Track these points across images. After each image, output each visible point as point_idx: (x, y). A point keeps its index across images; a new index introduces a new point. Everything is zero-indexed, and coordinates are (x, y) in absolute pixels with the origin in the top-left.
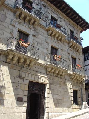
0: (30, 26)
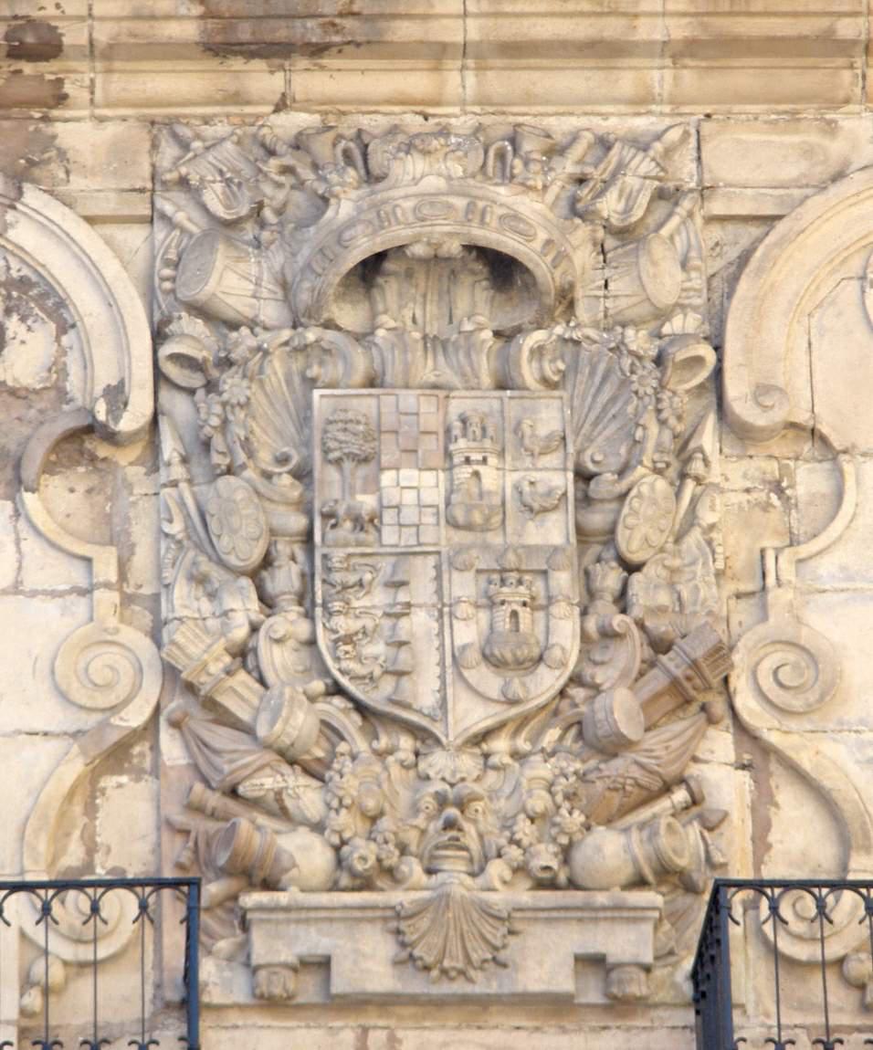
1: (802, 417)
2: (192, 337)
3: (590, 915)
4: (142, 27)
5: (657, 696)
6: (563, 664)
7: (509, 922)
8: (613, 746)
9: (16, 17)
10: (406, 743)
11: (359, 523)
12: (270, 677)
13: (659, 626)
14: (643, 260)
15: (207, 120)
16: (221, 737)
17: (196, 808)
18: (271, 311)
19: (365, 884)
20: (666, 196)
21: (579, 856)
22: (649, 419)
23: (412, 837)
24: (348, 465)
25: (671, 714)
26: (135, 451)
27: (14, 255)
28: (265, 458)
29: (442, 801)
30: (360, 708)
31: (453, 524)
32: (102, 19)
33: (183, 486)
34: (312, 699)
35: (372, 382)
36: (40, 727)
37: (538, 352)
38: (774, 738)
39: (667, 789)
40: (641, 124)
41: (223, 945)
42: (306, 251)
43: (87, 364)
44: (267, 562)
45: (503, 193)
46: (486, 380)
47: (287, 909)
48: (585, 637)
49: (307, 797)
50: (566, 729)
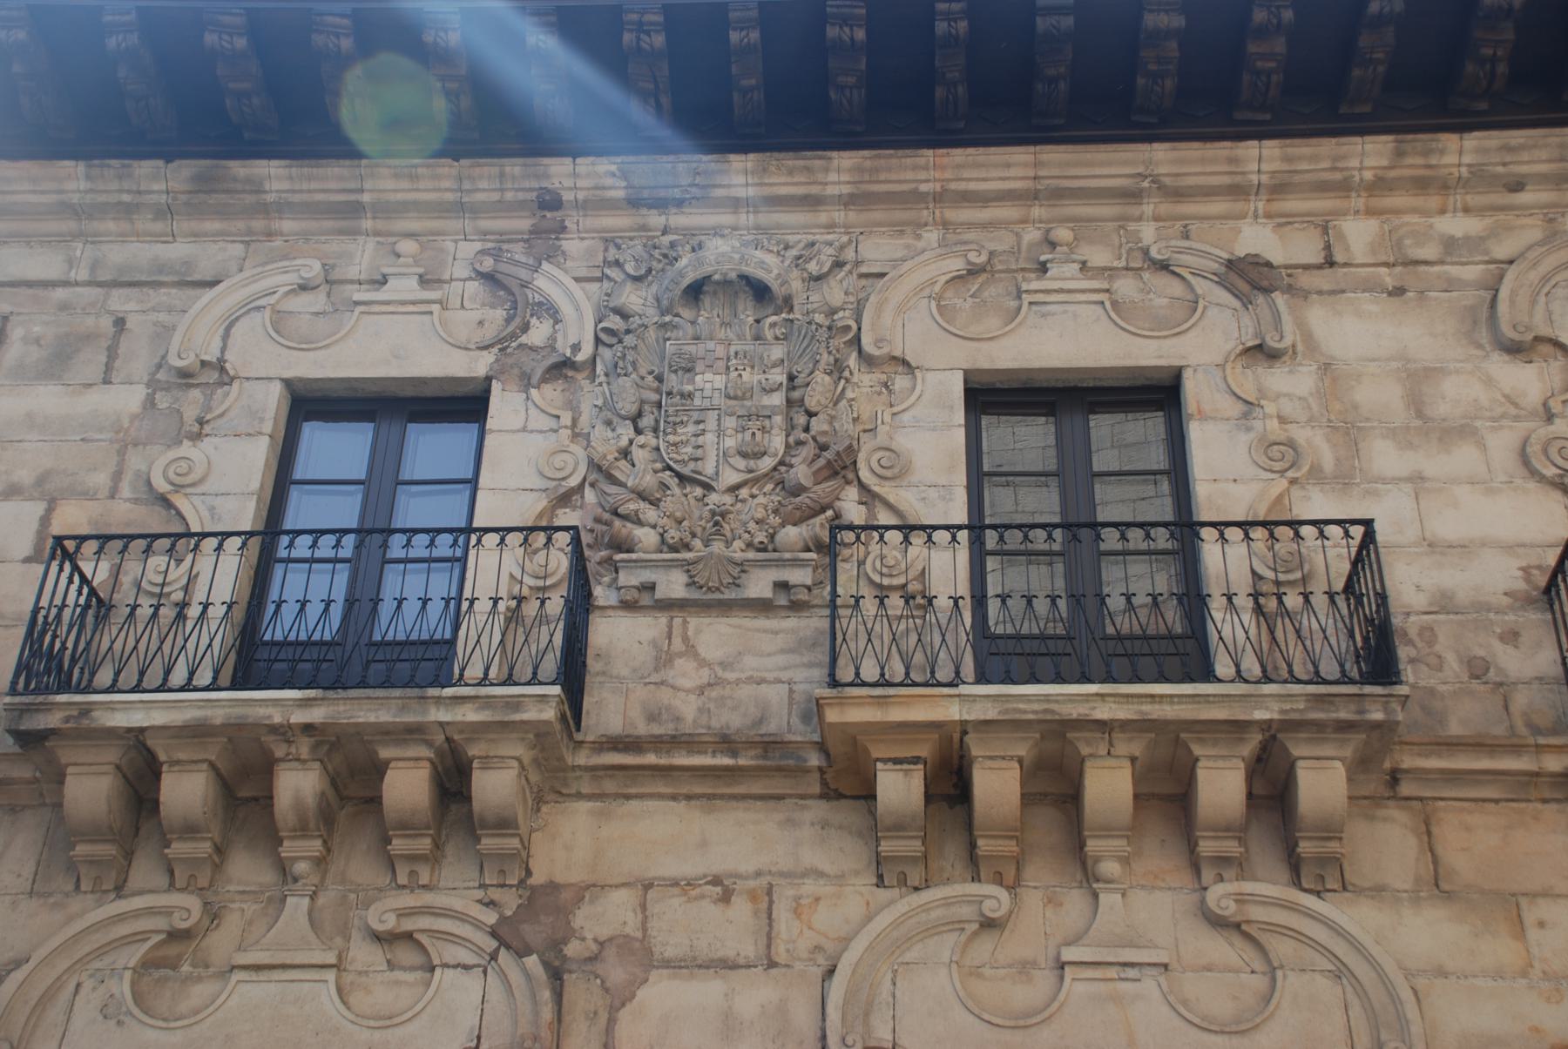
0: (1221, 895)
1: (897, 353)
2: (615, 322)
3: (781, 563)
4: (598, 192)
5: (820, 469)
6: (776, 455)
7: (743, 566)
8: (798, 490)
9: (541, 188)
10: (699, 491)
11: (682, 395)
12: (636, 462)
13: (822, 439)
14: (825, 286)
15: (631, 239)
16: (612, 489)
17: (597, 520)
18: (651, 311)
19: (674, 549)
20: (838, 265)
21: (778, 538)
22: (823, 350)
23: (698, 531)
24: (680, 373)
25: (826, 479)
26: (586, 373)
28: (643, 372)
29: (713, 513)
30: (679, 475)
31: (728, 397)
32: (581, 189)
33: (605, 385)
34: (656, 472)
35: (697, 338)
36: (529, 487)
37: (773, 325)
38: (876, 489)
39: (823, 510)
40: (830, 237)
41: (606, 579)
42: (666, 282)
43: (565, 336)
44: (640, 414)
45: (758, 253)
46: (748, 337)
47: (635, 561)
48: (787, 446)
49: (650, 514)
50: (777, 485)
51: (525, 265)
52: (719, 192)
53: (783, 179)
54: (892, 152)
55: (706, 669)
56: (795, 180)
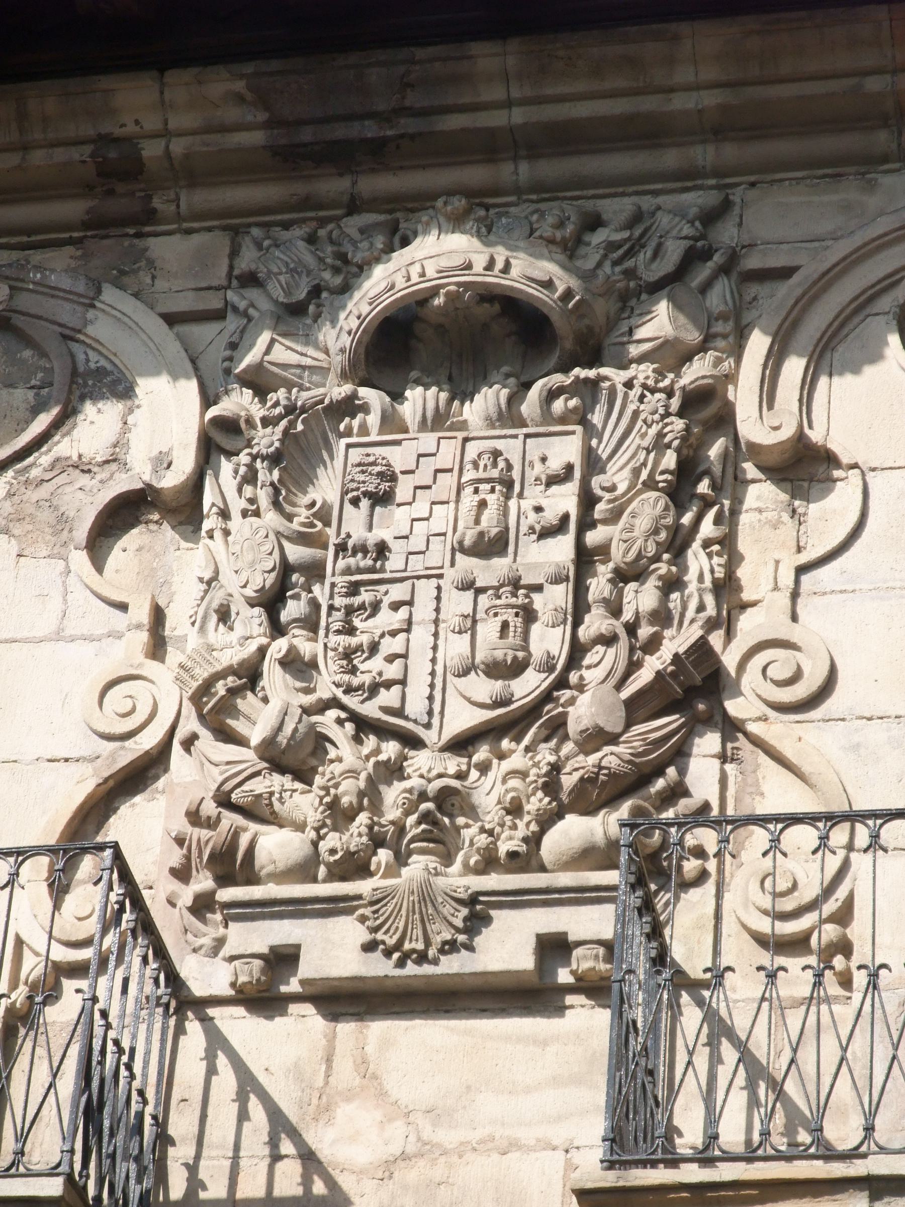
4: (216, 137)
27: (94, 349)
32: (180, 134)
51: (68, 295)
52: (455, 122)
53: (580, 86)
54: (803, 14)
55: (400, 1124)
56: (608, 85)
